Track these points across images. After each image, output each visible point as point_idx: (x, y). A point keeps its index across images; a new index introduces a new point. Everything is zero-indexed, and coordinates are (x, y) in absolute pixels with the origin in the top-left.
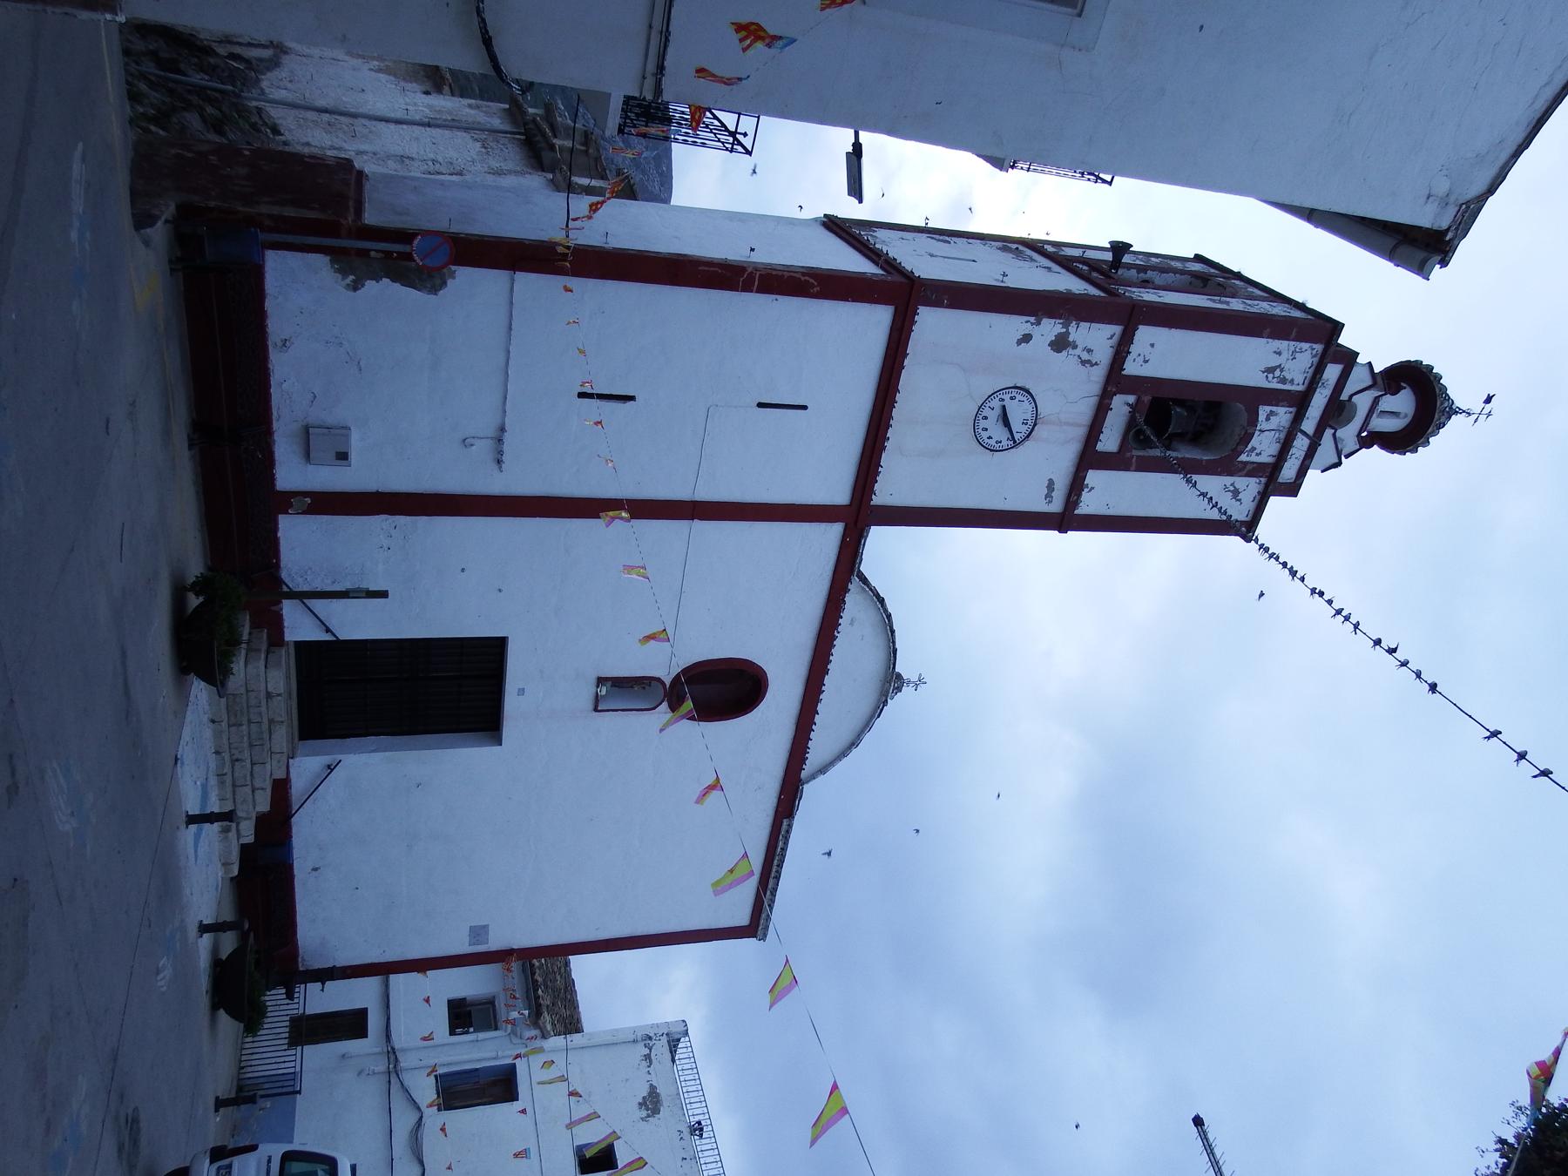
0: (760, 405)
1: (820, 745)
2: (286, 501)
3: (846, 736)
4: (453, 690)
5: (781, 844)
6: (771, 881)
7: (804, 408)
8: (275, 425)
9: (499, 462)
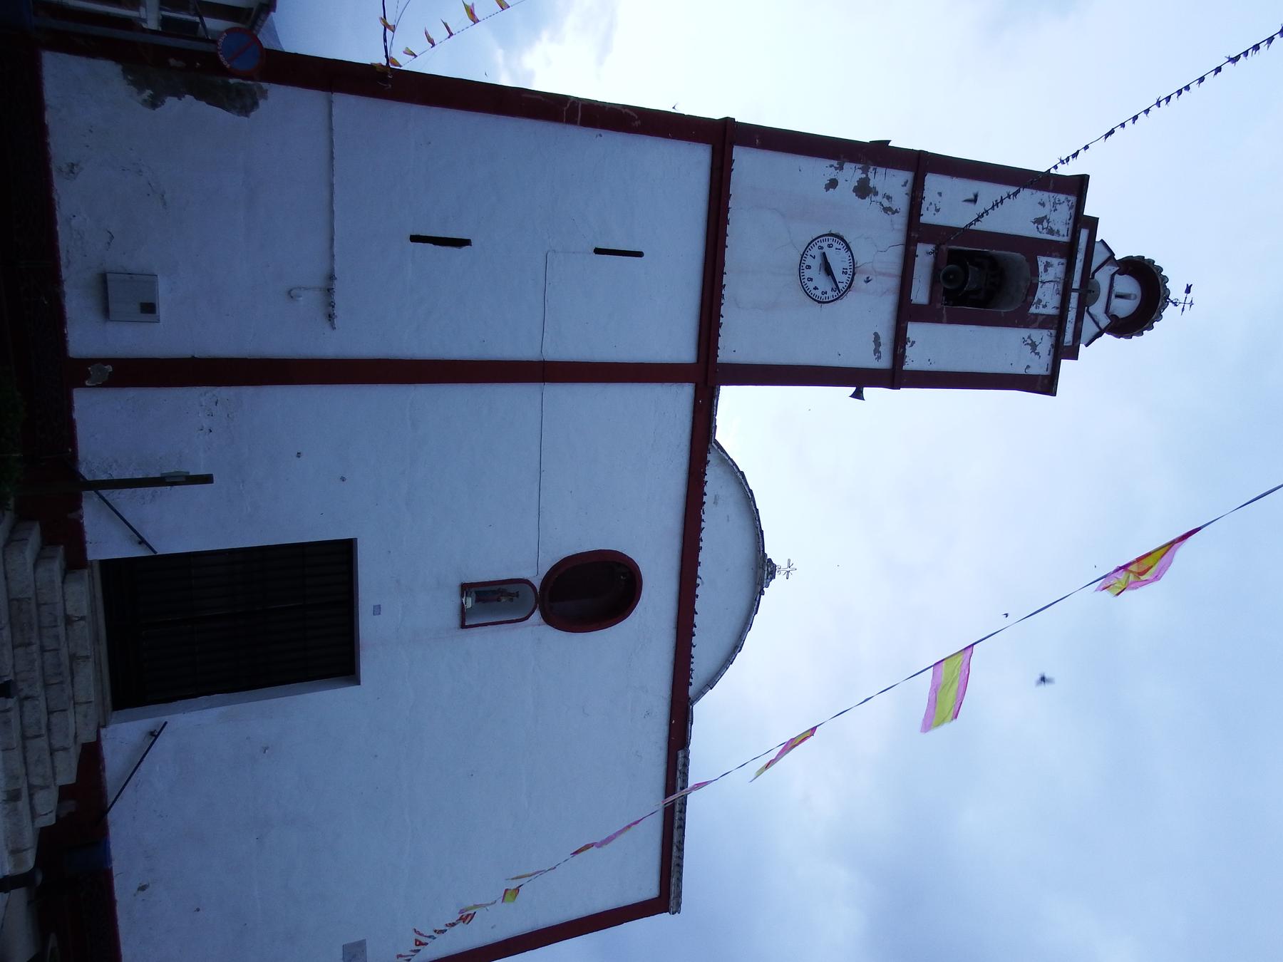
1: (696, 679)
2: (80, 372)
8: (65, 273)
9: (331, 317)
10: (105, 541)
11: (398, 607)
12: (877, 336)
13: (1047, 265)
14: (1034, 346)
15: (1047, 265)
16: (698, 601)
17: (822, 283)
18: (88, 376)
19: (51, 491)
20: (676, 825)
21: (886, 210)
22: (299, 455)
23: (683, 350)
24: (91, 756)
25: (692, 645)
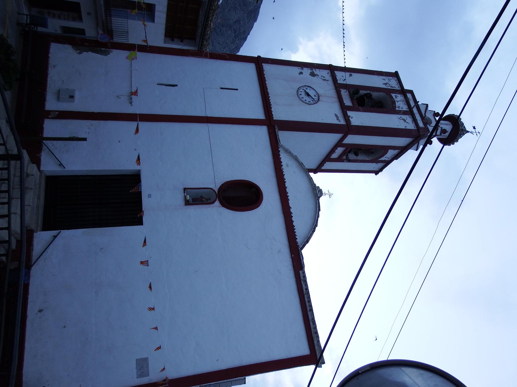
0: (221, 88)
1: (300, 233)
2: (48, 114)
3: (309, 222)
4: (115, 200)
5: (304, 286)
6: (309, 313)
7: (237, 90)
8: (48, 90)
9: (131, 103)
10: (49, 166)
11: (158, 196)
12: (336, 115)
13: (399, 107)
14: (405, 121)
15: (396, 96)
16: (286, 184)
17: (308, 99)
18: (50, 115)
19: (29, 127)
20: (308, 309)
21: (324, 80)
22: (119, 141)
23: (263, 130)
24: (28, 236)
25: (292, 221)
